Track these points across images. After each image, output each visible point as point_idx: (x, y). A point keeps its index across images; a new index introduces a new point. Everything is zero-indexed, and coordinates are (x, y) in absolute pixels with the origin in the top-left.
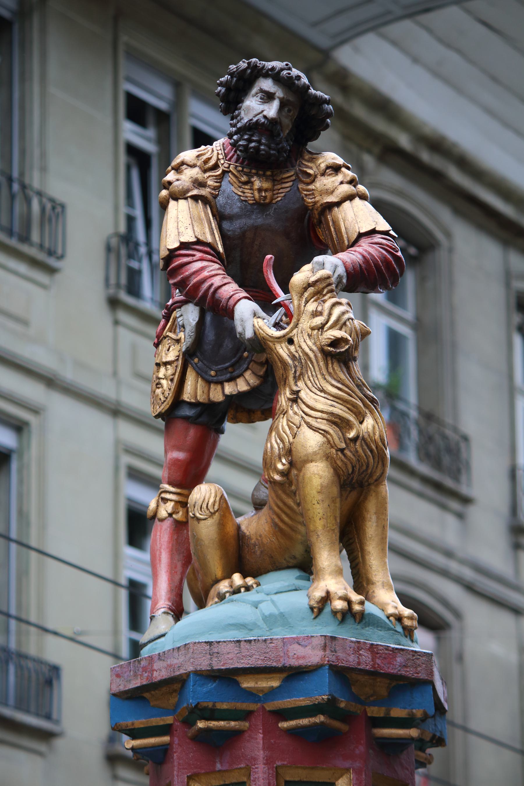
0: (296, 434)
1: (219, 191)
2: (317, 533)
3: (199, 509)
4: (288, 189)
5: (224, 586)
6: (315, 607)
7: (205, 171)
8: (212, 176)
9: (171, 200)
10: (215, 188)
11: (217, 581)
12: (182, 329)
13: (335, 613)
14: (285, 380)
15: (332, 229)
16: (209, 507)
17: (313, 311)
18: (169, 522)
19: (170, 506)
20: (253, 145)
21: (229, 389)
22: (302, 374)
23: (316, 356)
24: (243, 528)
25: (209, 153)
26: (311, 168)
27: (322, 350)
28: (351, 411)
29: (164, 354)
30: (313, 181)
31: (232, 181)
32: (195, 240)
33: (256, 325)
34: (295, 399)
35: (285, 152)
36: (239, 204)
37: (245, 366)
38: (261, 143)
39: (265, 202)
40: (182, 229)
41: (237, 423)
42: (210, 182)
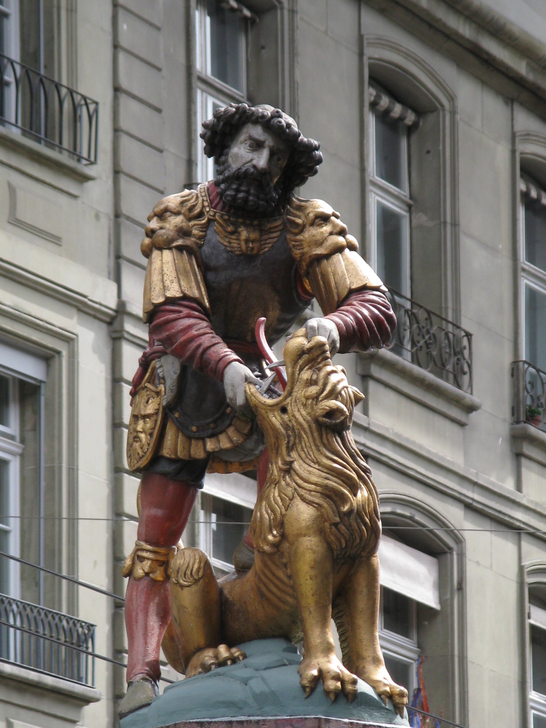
0: (289, 506)
1: (204, 241)
2: (309, 609)
3: (183, 576)
4: (276, 240)
5: (208, 656)
6: (307, 687)
7: (190, 219)
8: (198, 225)
9: (154, 249)
10: (200, 238)
11: (200, 649)
12: (162, 381)
13: (327, 693)
14: (278, 449)
15: (321, 283)
16: (193, 574)
17: (307, 379)
18: (146, 581)
19: (147, 565)
20: (241, 195)
21: (210, 445)
22: (294, 444)
23: (310, 426)
24: (226, 592)
25: (194, 199)
26: (299, 217)
27: (316, 421)
28: (346, 483)
29: (142, 407)
30: (301, 231)
31: (217, 230)
32: (181, 295)
33: (248, 391)
34: (288, 469)
35: (274, 202)
36: (225, 255)
37: (228, 422)
38: (246, 194)
39: (252, 253)
40: (167, 283)
41: (214, 473)
42: (195, 232)
